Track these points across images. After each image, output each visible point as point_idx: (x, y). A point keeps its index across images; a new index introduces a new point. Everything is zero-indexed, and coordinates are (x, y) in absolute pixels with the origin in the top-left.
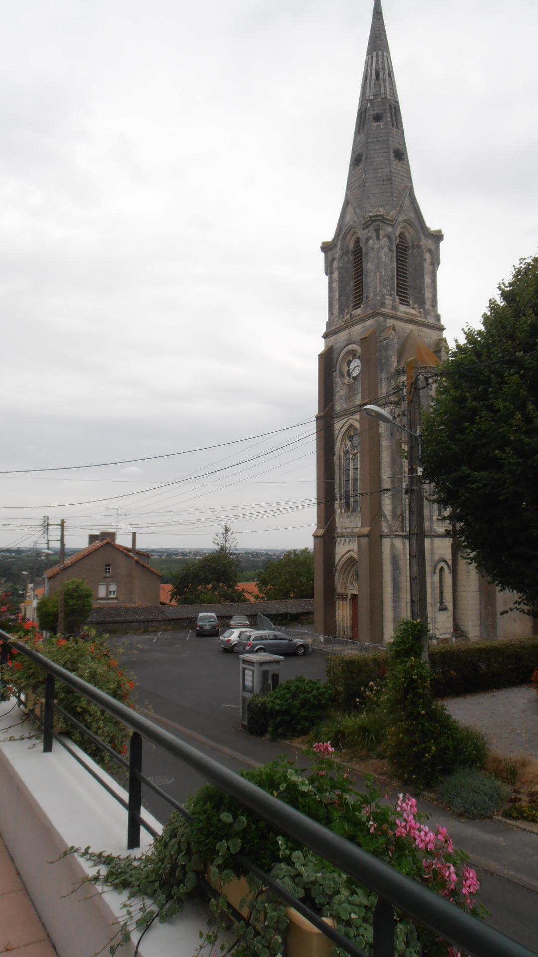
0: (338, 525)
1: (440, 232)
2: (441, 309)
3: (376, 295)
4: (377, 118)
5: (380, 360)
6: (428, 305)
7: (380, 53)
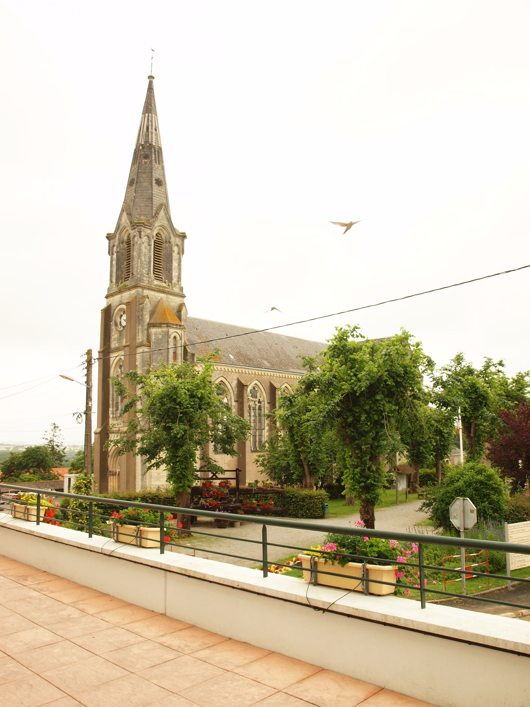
1: (184, 233)
2: (184, 283)
3: (138, 274)
4: (146, 157)
5: (139, 317)
6: (175, 280)
7: (150, 115)
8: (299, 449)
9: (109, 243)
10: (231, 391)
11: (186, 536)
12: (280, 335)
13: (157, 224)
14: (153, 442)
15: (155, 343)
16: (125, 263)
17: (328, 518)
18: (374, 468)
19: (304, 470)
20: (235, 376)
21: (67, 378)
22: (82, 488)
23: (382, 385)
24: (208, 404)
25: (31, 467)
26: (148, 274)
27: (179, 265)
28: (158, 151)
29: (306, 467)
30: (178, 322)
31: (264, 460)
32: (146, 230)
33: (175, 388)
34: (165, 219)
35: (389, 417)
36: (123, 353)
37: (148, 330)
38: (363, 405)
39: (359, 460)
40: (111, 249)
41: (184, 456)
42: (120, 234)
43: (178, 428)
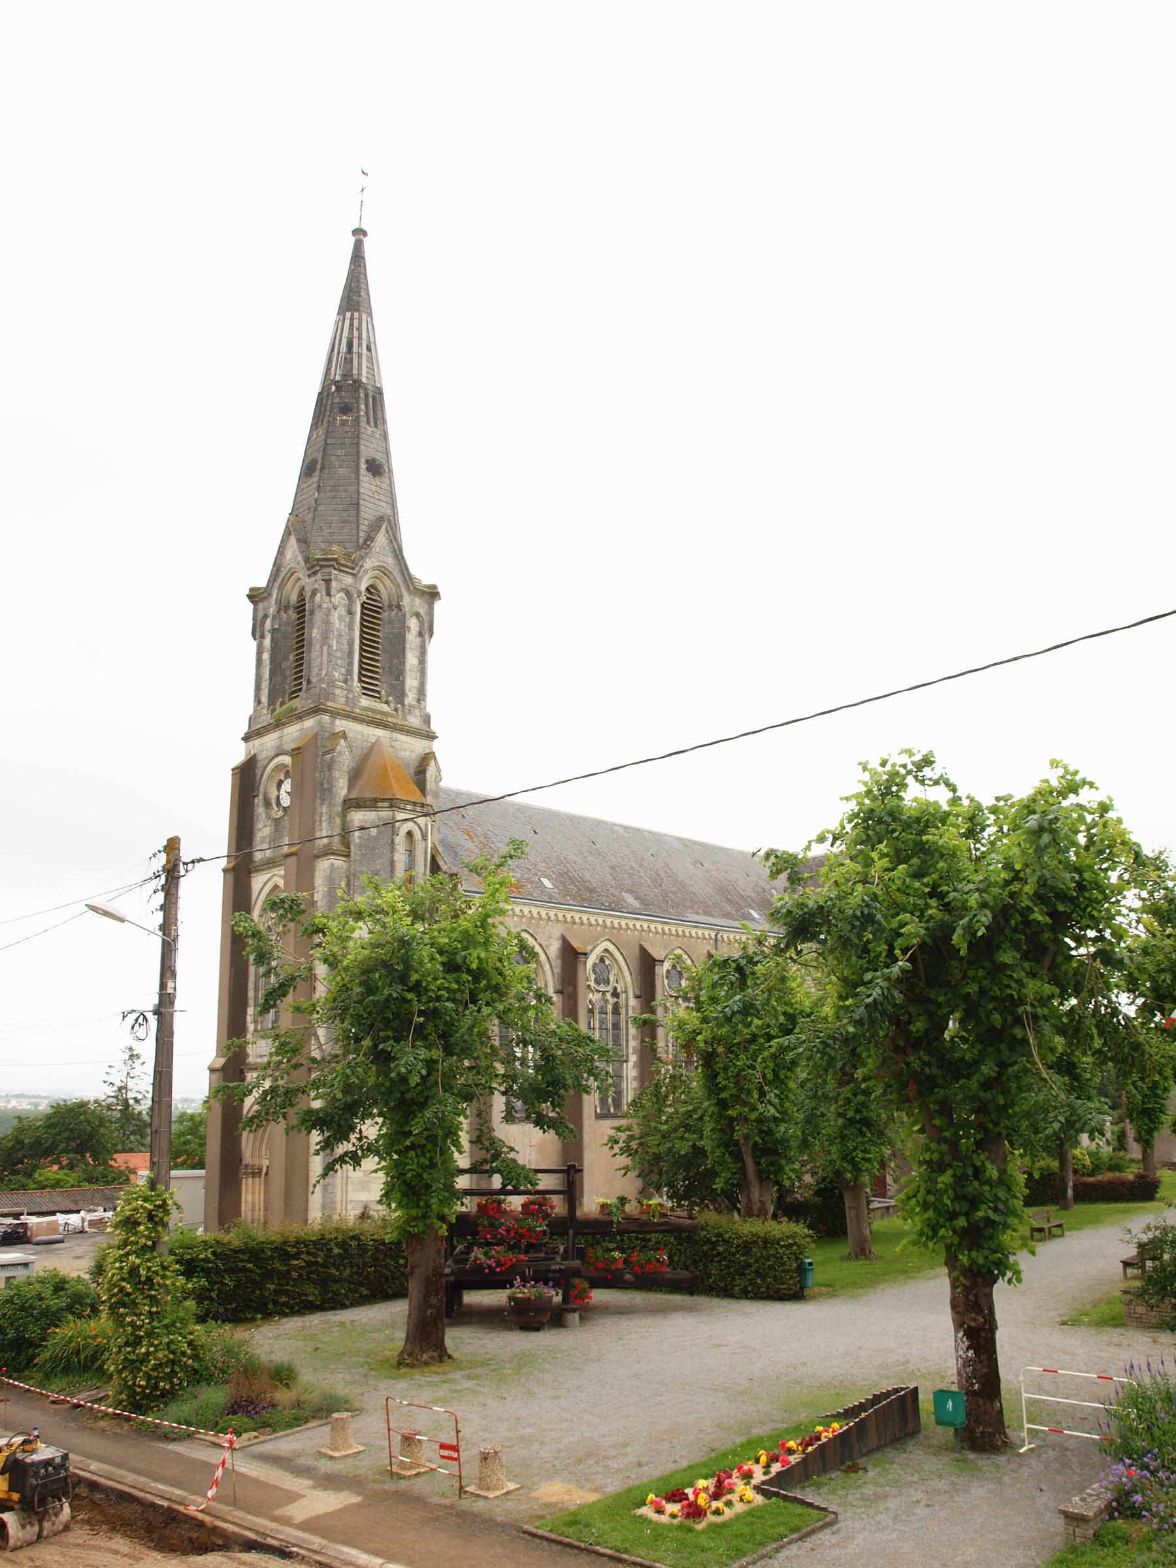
1: (435, 587)
2: (432, 705)
3: (322, 680)
4: (346, 409)
5: (322, 784)
6: (410, 698)
7: (356, 315)
8: (730, 1112)
9: (255, 611)
10: (547, 967)
11: (432, 1358)
12: (661, 835)
13: (369, 564)
14: (339, 1096)
15: (360, 846)
16: (292, 657)
17: (813, 1298)
18: (993, 1172)
19: (744, 1166)
20: (557, 931)
21: (106, 914)
22: (139, 1224)
23: (1013, 922)
24: (496, 988)
25: (63, 1151)
26: (346, 681)
27: (422, 661)
28: (374, 398)
30: (418, 798)
31: (631, 1138)
32: (341, 576)
33: (405, 943)
35: (1035, 1017)
36: (282, 872)
37: (344, 815)
38: (958, 982)
39: (944, 1147)
41: (426, 1133)
42: (281, 588)
43: (411, 1058)
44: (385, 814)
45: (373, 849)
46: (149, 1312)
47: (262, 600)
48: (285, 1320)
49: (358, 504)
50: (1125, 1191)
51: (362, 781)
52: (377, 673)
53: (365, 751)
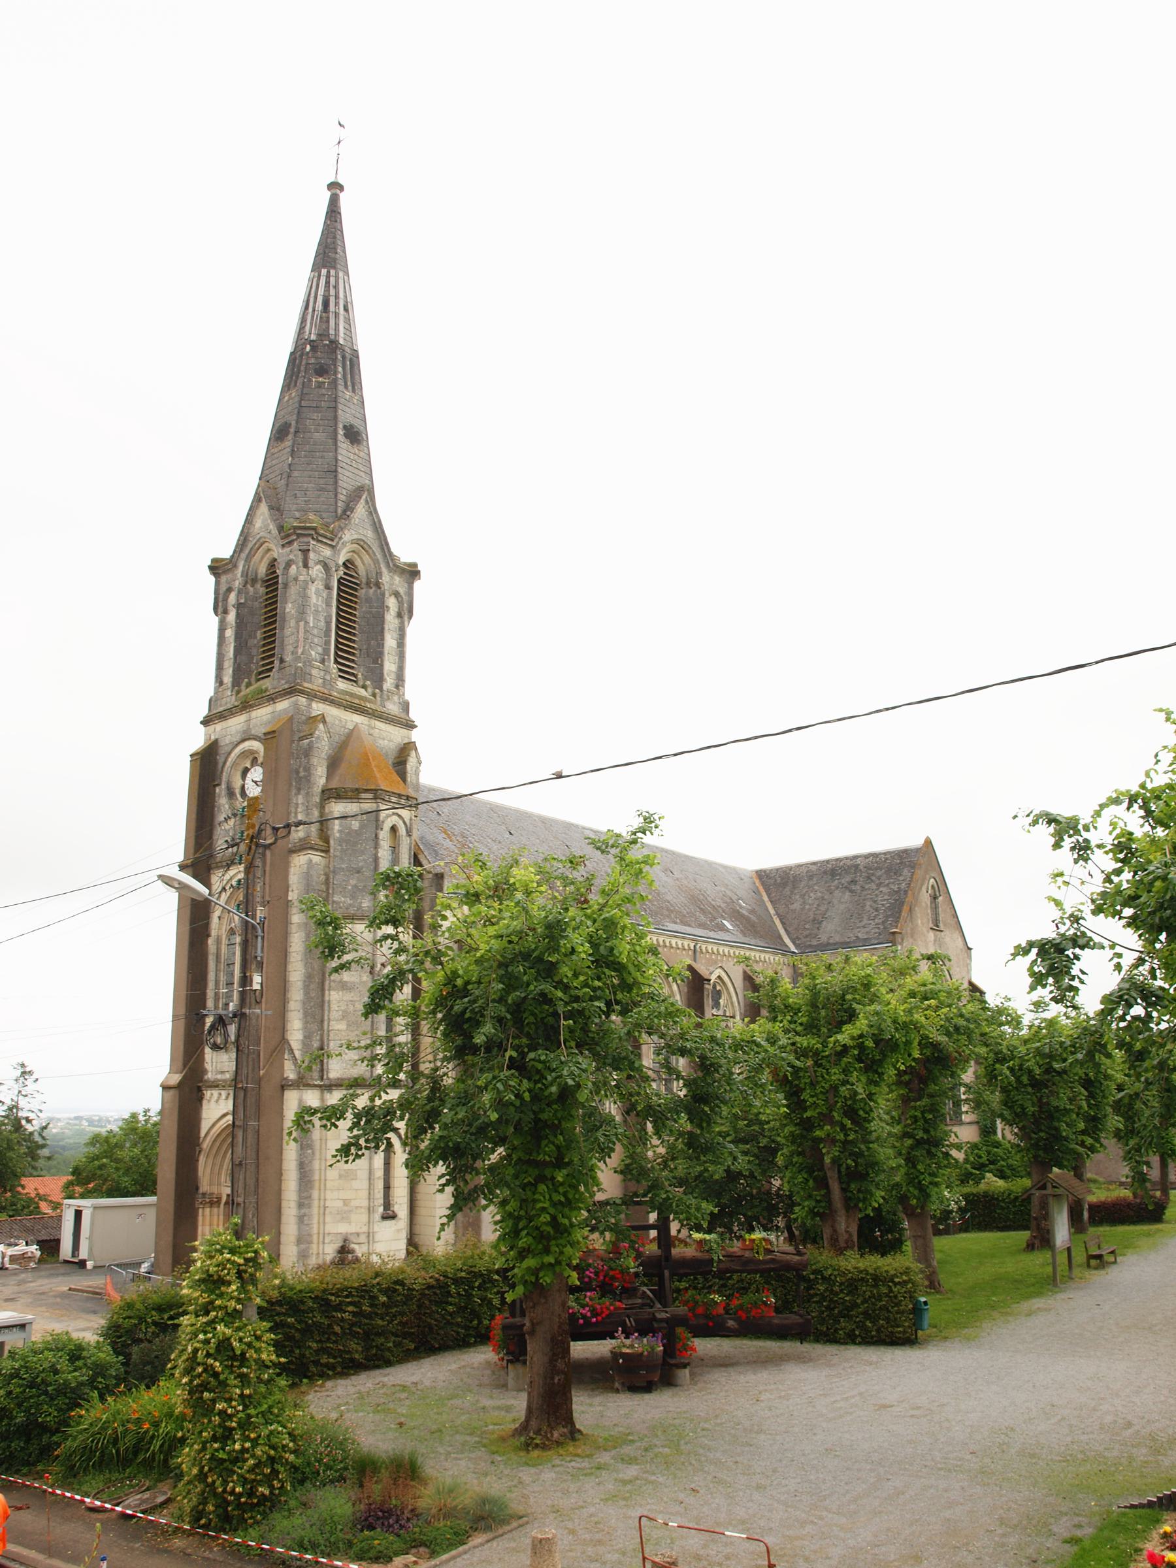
0: (208, 1066)
1: (415, 565)
2: (410, 692)
3: (298, 659)
4: (321, 371)
5: (298, 772)
6: (389, 683)
9: (217, 584)
13: (348, 536)
15: (340, 841)
19: (829, 1192)
22: (229, 1283)
26: (323, 661)
27: (401, 644)
28: (351, 360)
29: (835, 1187)
34: (368, 525)
37: (322, 807)
40: (221, 599)
44: (368, 806)
45: (355, 844)
46: (242, 1395)
47: (226, 572)
48: (329, 1384)
49: (336, 471)
50: (1132, 1213)
51: (342, 769)
52: (353, 654)
53: (343, 738)
